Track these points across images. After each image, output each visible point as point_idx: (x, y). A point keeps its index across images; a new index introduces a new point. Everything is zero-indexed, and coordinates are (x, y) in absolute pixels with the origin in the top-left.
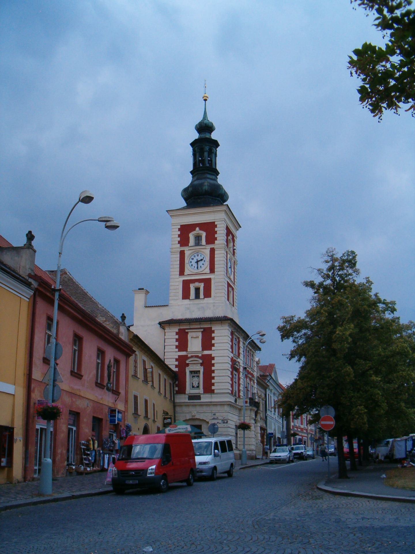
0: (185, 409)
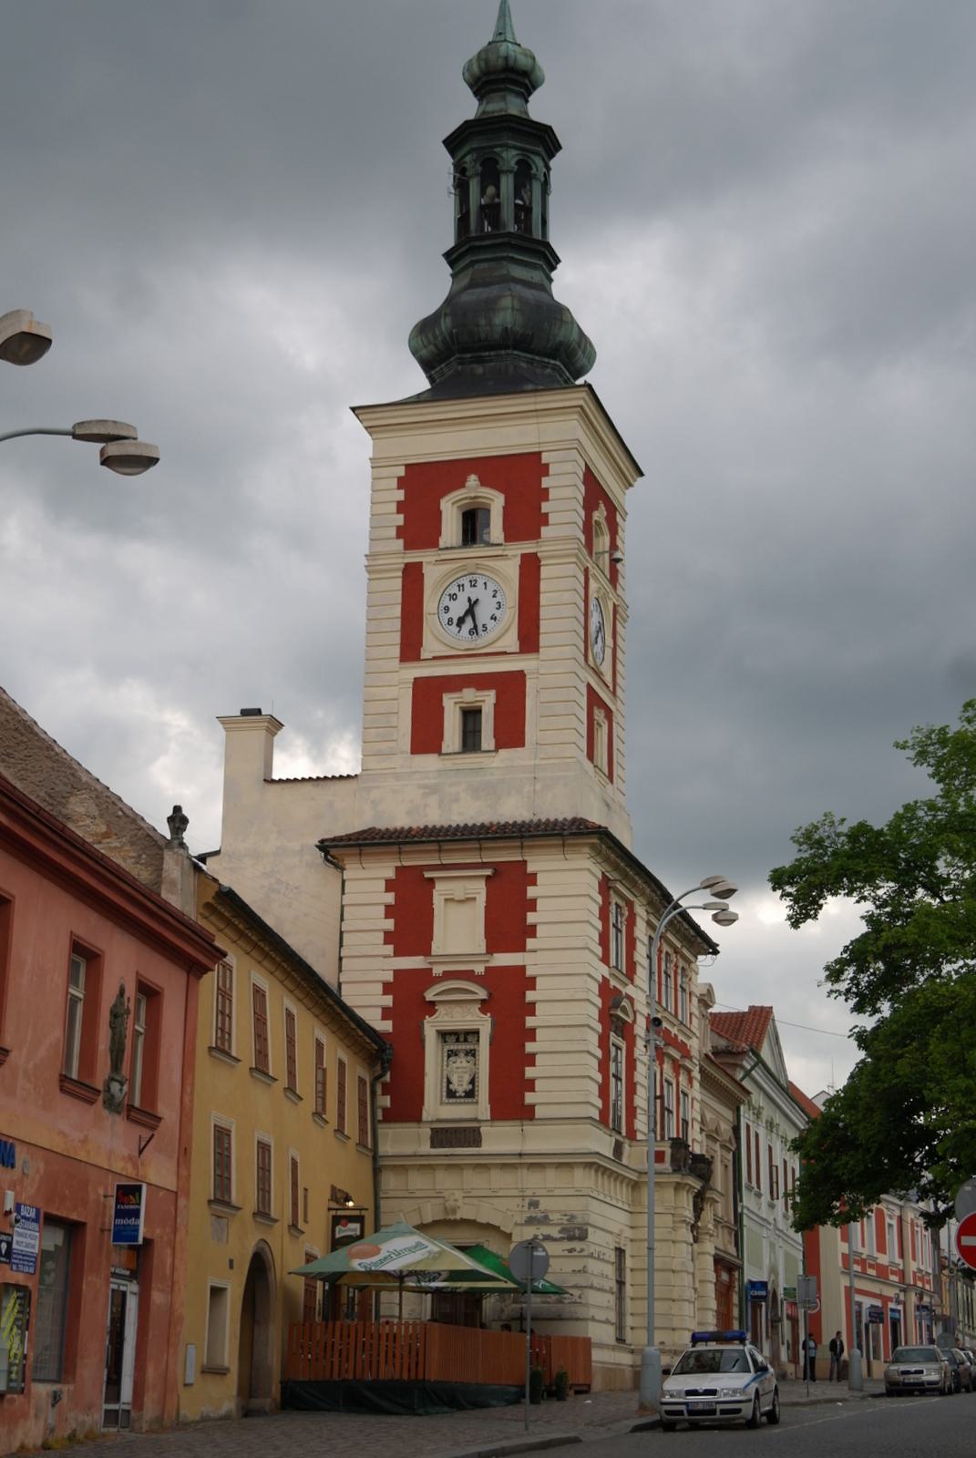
0: (418, 1181)
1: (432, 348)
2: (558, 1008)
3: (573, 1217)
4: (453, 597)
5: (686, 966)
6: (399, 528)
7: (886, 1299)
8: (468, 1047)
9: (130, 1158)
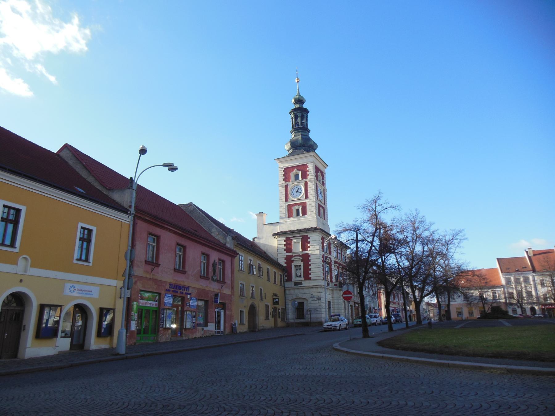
0: (292, 291)
1: (288, 148)
2: (314, 260)
3: (318, 296)
4: (294, 190)
5: (320, 167)
6: (284, 179)
7: (395, 308)
8: (300, 268)
9: (219, 289)
